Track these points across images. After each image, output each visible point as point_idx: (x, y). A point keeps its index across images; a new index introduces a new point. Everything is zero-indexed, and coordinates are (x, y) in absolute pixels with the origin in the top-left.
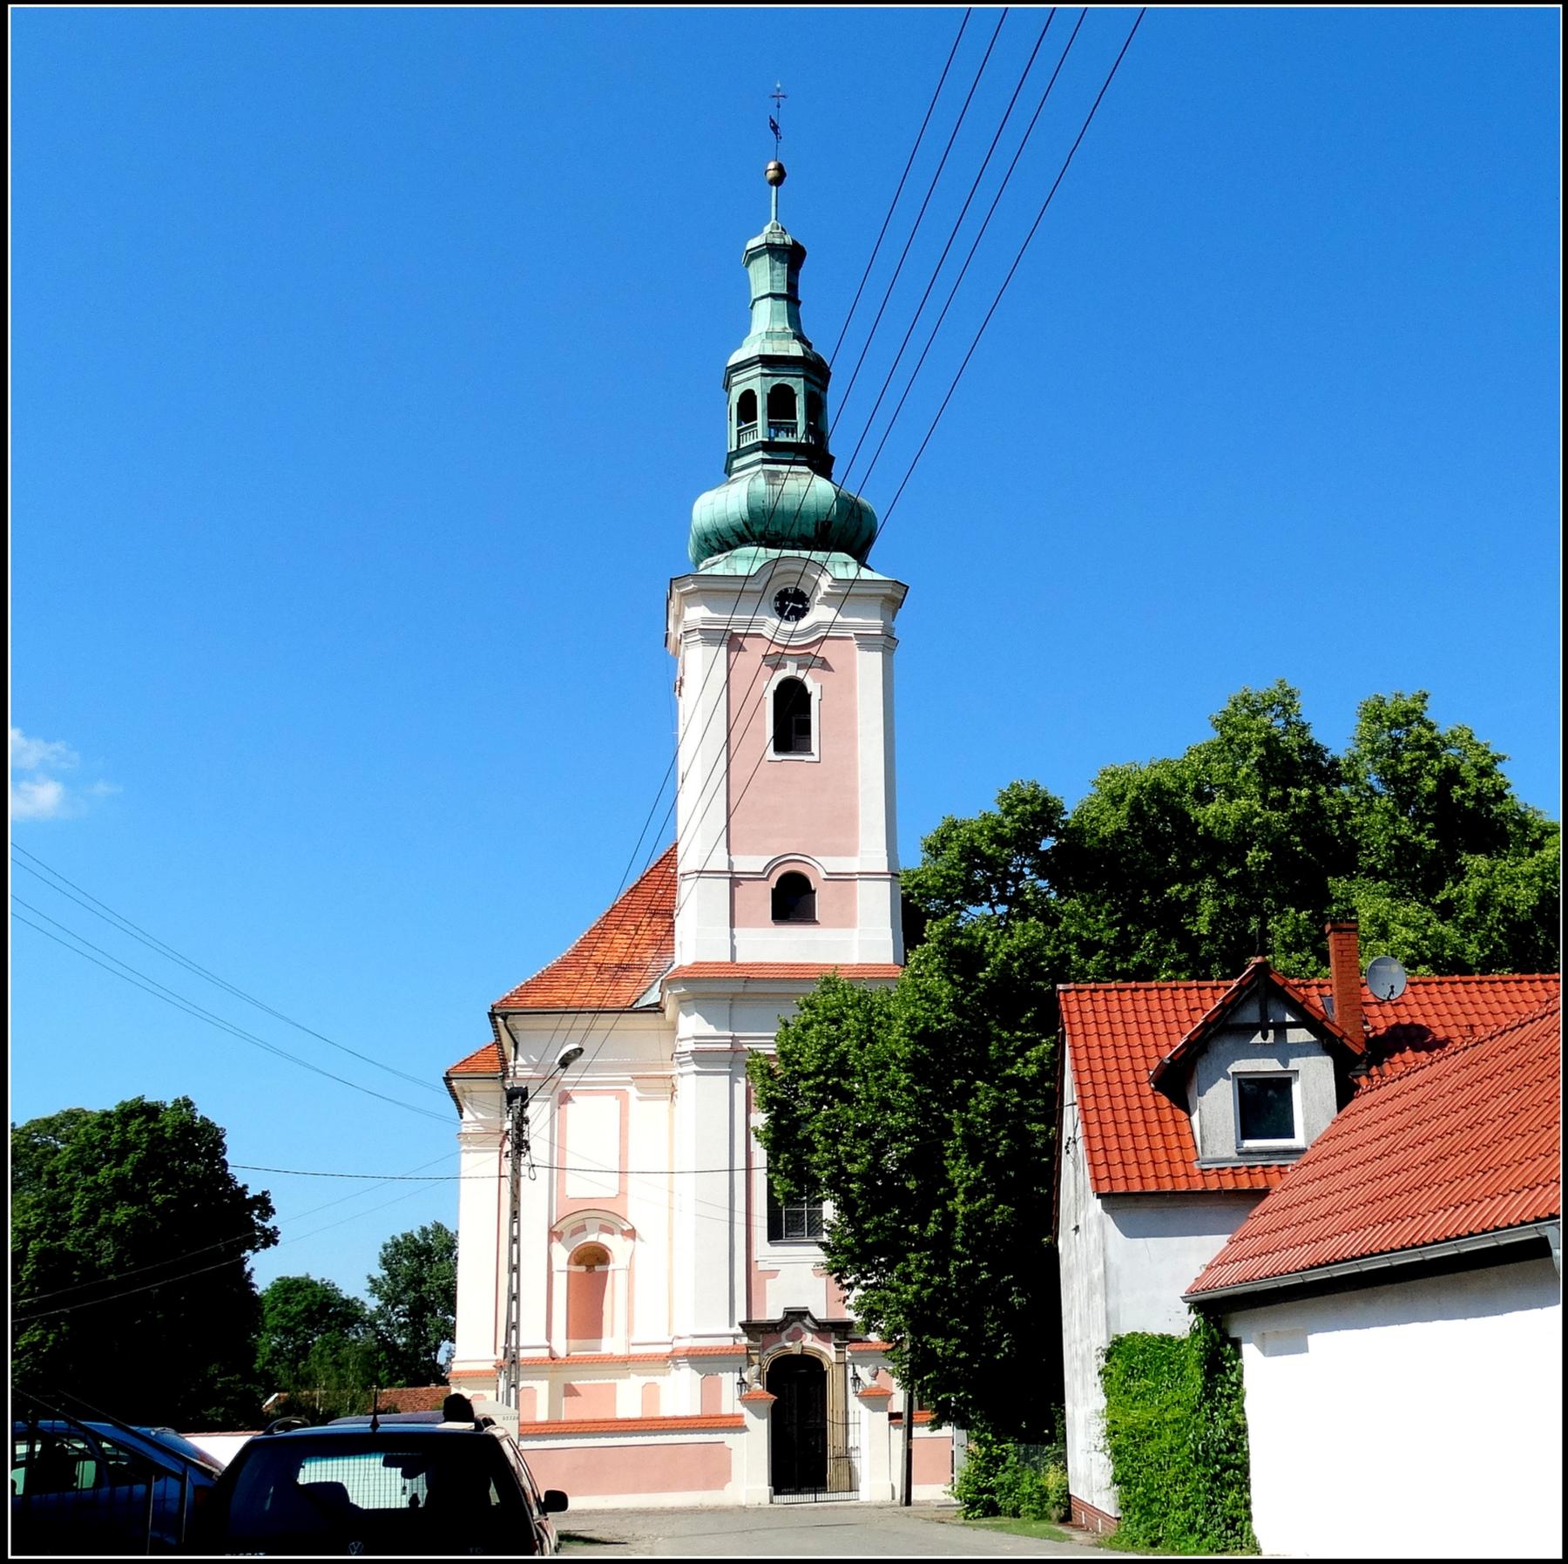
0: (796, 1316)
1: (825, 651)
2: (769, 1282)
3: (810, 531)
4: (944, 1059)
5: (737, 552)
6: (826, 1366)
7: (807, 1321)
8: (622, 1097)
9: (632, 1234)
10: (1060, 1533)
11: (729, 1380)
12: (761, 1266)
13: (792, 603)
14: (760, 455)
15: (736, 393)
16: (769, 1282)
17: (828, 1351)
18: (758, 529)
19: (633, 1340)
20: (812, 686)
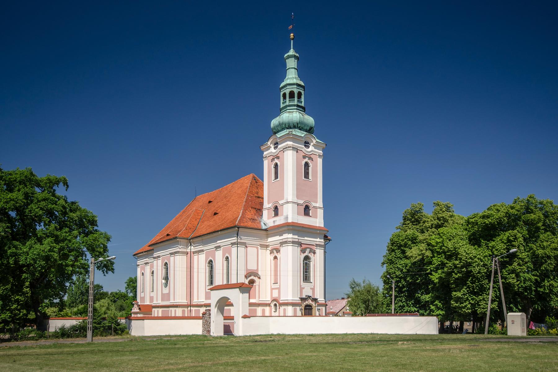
1: (312, 156)
3: (308, 129)
4: (87, 269)
5: (296, 130)
8: (257, 248)
9: (259, 278)
10: (444, 339)
11: (298, 308)
13: (307, 144)
14: (296, 107)
15: (282, 93)
17: (313, 304)
18: (299, 125)
20: (311, 164)
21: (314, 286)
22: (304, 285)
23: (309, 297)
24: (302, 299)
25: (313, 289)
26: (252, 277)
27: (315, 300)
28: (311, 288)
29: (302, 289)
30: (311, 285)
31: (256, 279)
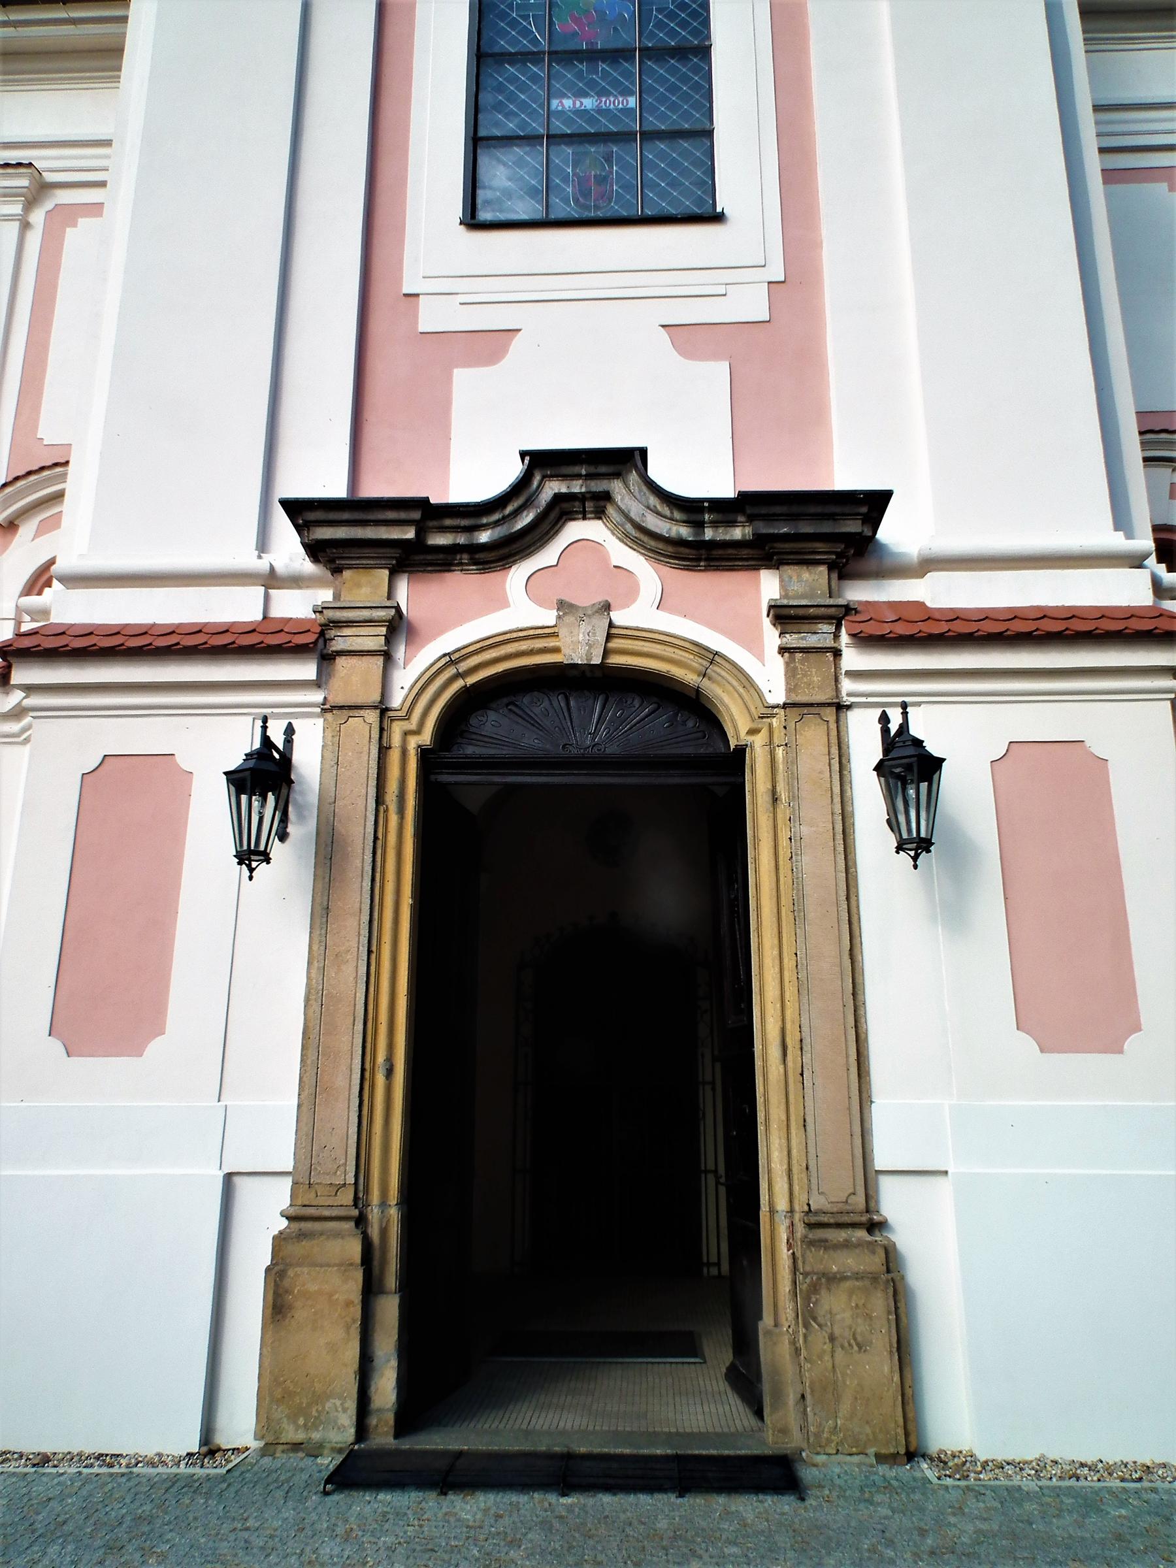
0: (577, 480)
2: (467, 383)
6: (738, 725)
7: (626, 495)
16: (467, 383)
21: (797, 286)
24: (337, 531)
25: (774, 355)
27: (830, 531)
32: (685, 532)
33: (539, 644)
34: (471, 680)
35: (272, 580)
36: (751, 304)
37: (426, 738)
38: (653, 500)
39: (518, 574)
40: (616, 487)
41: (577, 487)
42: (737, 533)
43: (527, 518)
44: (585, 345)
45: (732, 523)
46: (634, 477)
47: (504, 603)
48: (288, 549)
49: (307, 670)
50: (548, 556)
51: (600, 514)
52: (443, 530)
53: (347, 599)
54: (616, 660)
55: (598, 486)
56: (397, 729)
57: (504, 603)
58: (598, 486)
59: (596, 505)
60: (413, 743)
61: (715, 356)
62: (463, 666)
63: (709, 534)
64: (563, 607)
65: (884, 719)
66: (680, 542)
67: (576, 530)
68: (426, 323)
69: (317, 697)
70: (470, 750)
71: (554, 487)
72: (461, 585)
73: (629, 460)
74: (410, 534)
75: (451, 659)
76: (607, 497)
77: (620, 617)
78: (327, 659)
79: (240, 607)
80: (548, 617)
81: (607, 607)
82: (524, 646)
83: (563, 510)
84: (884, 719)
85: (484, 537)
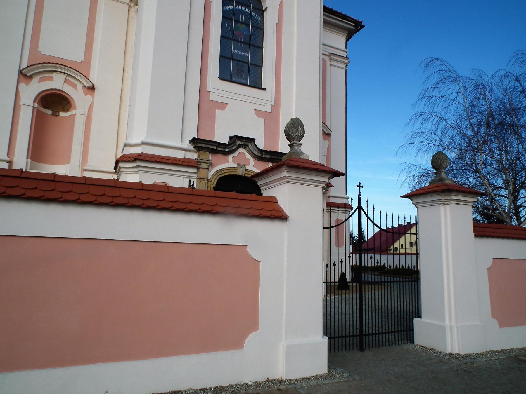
12: (213, 97)
19: (85, 168)
21: (276, 107)
22: (219, 89)
23: (246, 142)
26: (57, 83)
28: (258, 113)
29: (207, 108)
30: (263, 99)
31: (76, 94)
32: (260, 155)
33: (234, 170)
34: (222, 176)
35: (185, 150)
36: (268, 109)
37: (214, 185)
38: (255, 148)
39: (230, 157)
40: (249, 144)
41: (243, 143)
42: (268, 156)
43: (234, 147)
44: (239, 114)
45: (267, 155)
46: (253, 143)
47: (228, 162)
48: (191, 147)
49: (195, 170)
50: (236, 154)
51: (245, 148)
52: (220, 147)
53: (201, 157)
54: (246, 175)
55: (247, 144)
56: (210, 183)
57: (228, 162)
58: (247, 144)
59: (245, 146)
60: (212, 186)
61: (262, 117)
62: (221, 173)
63: (263, 156)
64: (238, 164)
65: (190, 181)
66: (259, 156)
67: (242, 150)
68: (211, 98)
69: (196, 176)
70: (475, 200)
71: (239, 142)
72: (221, 157)
73: (252, 140)
74: (215, 148)
75: (219, 171)
76: (247, 145)
77: (247, 167)
78: (198, 168)
79: (181, 155)
80: (236, 166)
81: (245, 165)
82: (232, 170)
83: (240, 146)
84: (190, 181)
85: (227, 150)
